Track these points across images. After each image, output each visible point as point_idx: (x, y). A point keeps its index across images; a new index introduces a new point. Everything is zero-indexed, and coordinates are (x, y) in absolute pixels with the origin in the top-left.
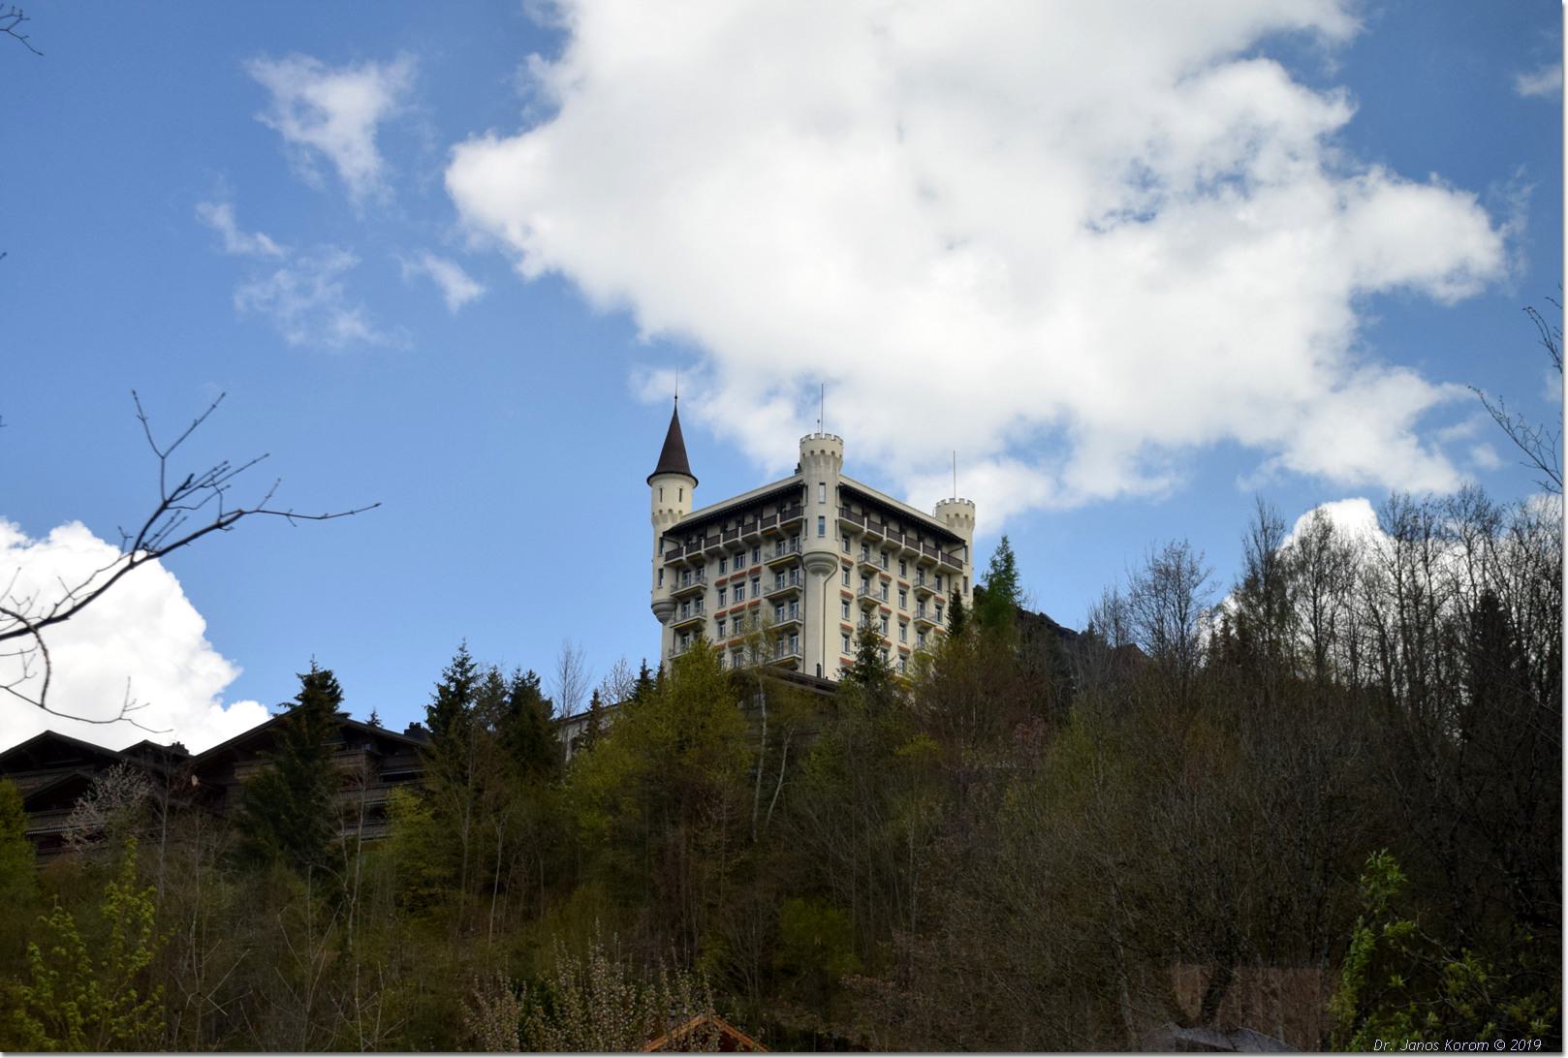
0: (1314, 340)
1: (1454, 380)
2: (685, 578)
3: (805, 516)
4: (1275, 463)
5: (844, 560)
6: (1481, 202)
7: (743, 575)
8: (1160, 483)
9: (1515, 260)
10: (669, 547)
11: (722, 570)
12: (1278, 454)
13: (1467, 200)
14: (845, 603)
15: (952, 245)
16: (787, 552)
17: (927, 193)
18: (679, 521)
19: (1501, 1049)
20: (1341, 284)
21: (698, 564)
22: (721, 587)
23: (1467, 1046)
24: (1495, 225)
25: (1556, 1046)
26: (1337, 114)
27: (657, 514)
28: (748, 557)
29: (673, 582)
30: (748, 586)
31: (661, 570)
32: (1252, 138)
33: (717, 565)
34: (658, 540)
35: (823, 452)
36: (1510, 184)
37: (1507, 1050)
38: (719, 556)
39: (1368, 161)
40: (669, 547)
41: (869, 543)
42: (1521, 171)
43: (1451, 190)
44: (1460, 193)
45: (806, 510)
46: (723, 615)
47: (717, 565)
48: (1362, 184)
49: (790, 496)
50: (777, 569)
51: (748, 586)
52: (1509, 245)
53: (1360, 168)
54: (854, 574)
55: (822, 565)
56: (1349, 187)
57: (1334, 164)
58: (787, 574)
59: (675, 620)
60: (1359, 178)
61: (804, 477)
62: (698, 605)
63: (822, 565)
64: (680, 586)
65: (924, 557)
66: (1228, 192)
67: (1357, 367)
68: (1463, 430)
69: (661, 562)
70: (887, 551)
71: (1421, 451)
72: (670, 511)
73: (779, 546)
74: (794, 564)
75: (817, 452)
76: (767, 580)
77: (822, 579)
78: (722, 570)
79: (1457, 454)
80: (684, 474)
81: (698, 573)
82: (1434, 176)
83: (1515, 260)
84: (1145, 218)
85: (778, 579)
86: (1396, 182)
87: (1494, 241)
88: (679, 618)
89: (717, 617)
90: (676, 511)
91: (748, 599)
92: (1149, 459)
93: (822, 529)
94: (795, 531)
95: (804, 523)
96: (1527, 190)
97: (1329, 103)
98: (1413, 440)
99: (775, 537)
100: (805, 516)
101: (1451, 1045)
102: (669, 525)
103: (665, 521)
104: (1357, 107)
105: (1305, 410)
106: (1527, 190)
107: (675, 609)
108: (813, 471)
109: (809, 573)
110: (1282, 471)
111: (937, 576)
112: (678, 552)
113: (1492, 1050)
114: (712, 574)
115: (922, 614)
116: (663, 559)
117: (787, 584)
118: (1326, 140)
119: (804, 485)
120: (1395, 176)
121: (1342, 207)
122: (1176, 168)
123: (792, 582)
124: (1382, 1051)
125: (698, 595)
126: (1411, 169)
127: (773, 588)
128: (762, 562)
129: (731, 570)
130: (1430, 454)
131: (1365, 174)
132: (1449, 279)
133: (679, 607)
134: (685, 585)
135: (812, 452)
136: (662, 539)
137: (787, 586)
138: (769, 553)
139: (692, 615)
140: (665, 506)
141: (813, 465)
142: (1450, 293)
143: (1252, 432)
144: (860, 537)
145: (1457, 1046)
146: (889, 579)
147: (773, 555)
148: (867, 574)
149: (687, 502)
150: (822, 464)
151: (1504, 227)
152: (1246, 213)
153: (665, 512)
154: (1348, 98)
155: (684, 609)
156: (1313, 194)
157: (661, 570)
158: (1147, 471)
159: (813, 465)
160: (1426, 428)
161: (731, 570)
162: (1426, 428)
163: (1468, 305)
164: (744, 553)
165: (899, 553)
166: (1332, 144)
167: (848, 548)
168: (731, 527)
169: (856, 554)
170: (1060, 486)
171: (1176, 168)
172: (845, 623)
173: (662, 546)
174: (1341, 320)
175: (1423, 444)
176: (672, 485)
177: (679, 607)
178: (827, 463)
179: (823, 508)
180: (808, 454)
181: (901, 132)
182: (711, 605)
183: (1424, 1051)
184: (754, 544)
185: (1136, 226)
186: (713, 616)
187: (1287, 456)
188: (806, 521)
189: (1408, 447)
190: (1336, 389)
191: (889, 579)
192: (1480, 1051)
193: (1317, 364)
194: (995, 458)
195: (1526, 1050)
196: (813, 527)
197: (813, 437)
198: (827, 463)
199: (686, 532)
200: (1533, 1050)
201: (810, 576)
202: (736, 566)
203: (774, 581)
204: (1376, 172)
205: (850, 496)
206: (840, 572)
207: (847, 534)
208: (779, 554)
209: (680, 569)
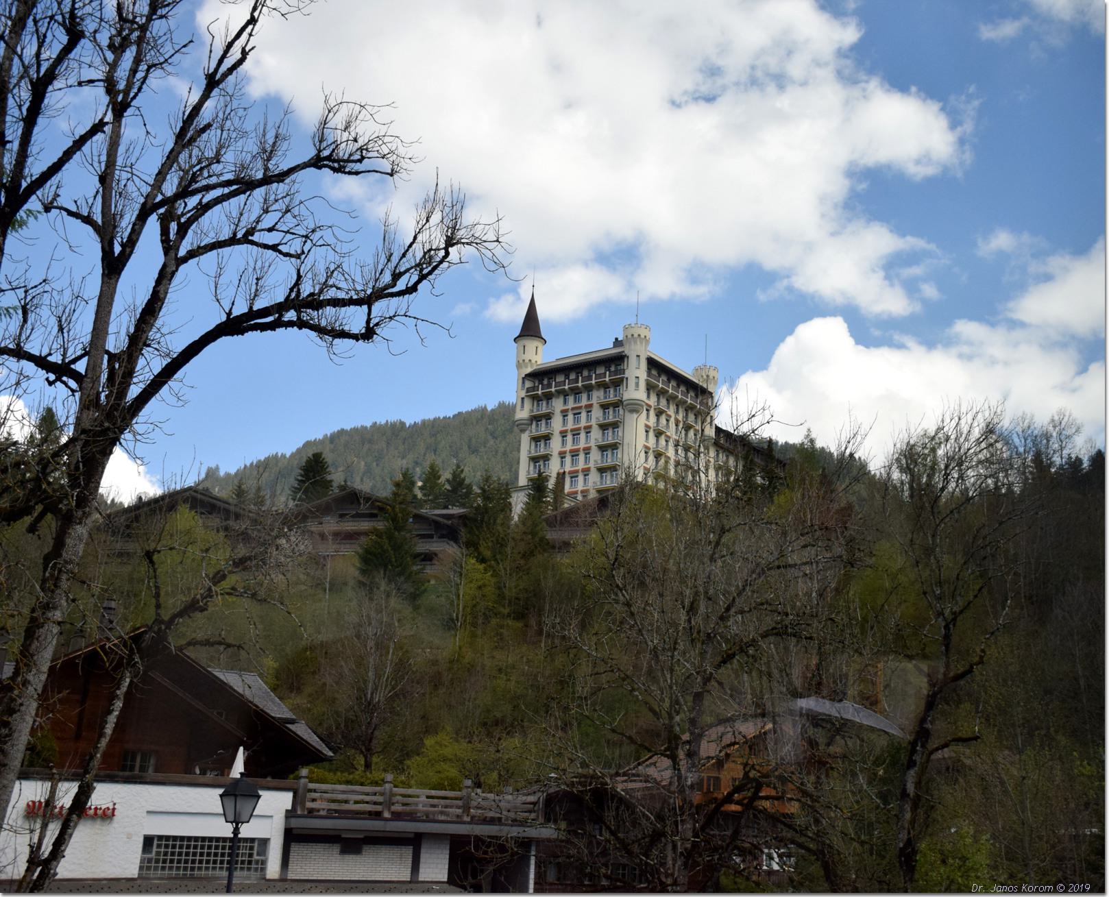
0: (822, 199)
1: (913, 235)
2: (538, 405)
3: (626, 376)
4: (785, 282)
5: (647, 405)
6: (943, 109)
7: (580, 408)
8: (702, 291)
9: (963, 152)
10: (528, 384)
11: (565, 402)
12: (788, 277)
13: (934, 107)
14: (647, 431)
15: (569, 105)
16: (612, 397)
17: (557, 67)
18: (535, 367)
19: (1062, 890)
20: (841, 156)
21: (548, 397)
22: (564, 413)
23: (1037, 888)
24: (953, 125)
25: (1102, 890)
26: (849, 34)
27: (521, 362)
28: (584, 396)
29: (530, 407)
30: (584, 415)
31: (523, 399)
32: (787, 47)
33: (561, 400)
34: (521, 381)
35: (639, 335)
36: (963, 97)
37: (1066, 892)
38: (565, 394)
39: (871, 72)
40: (528, 384)
41: (661, 393)
42: (972, 89)
43: (924, 100)
44: (929, 101)
45: (627, 372)
46: (566, 431)
47: (561, 400)
48: (864, 90)
49: (615, 361)
50: (604, 407)
51: (584, 415)
52: (962, 142)
53: (865, 78)
54: (652, 413)
55: (635, 407)
56: (856, 92)
57: (847, 72)
58: (611, 410)
59: (531, 431)
60: (863, 85)
61: (626, 350)
62: (547, 423)
63: (635, 407)
64: (535, 410)
65: (662, 388)
66: (771, 88)
67: (850, 220)
68: (916, 271)
69: (523, 394)
70: (671, 399)
71: (887, 282)
72: (530, 360)
73: (605, 392)
74: (616, 405)
75: (636, 335)
76: (597, 413)
77: (635, 416)
78: (565, 402)
79: (911, 288)
80: (536, 336)
81: (548, 403)
82: (913, 89)
83: (963, 152)
84: (710, 99)
85: (604, 413)
86: (888, 91)
87: (950, 138)
88: (534, 431)
89: (561, 432)
90: (533, 361)
91: (583, 423)
92: (695, 272)
93: (637, 385)
94: (618, 383)
95: (625, 380)
96: (976, 103)
97: (844, 25)
98: (882, 274)
99: (604, 386)
100: (626, 376)
101: (1027, 888)
102: (529, 370)
103: (526, 367)
104: (863, 31)
105: (809, 247)
106: (976, 103)
107: (531, 424)
108: (633, 347)
109: (626, 412)
110: (790, 289)
111: (695, 415)
112: (534, 388)
113: (1055, 891)
114: (558, 405)
115: (658, 425)
116: (525, 391)
117: (611, 417)
118: (841, 53)
119: (625, 356)
120: (887, 86)
121: (847, 102)
122: (735, 65)
123: (615, 417)
124: (977, 892)
125: (548, 417)
126: (899, 82)
127: (601, 419)
128: (594, 401)
129: (571, 403)
130: (892, 285)
131: (867, 82)
132: (918, 162)
133: (534, 423)
134: (538, 410)
135: (633, 335)
136: (523, 378)
137: (611, 419)
138: (598, 396)
139: (543, 430)
140: (527, 357)
141: (633, 343)
142: (920, 172)
143: (772, 259)
144: (667, 396)
145: (1031, 889)
146: (670, 416)
147: (602, 398)
148: (659, 413)
149: (543, 356)
150: (638, 343)
151: (959, 129)
152: (783, 102)
153: (527, 361)
154: (858, 25)
155: (537, 425)
156: (830, 93)
157: (523, 399)
158: (694, 281)
159: (633, 343)
160: (892, 267)
161: (571, 403)
162: (892, 267)
163: (930, 181)
164: (581, 393)
165: (658, 389)
166: (846, 57)
167: (648, 397)
168: (573, 376)
169: (653, 401)
170: (630, 286)
171: (735, 65)
172: (646, 444)
173: (523, 383)
174: (839, 187)
175: (887, 277)
176: (531, 344)
177: (534, 423)
178: (641, 343)
179: (637, 372)
180: (521, 362)
181: (539, 22)
182: (557, 424)
183: (1007, 892)
184: (589, 389)
185: (702, 104)
186: (558, 432)
187: (794, 279)
188: (627, 378)
189: (877, 279)
190: (833, 234)
191: (670, 416)
192: (1047, 892)
193: (823, 216)
194: (586, 264)
195: (1079, 892)
196: (632, 383)
197: (633, 325)
198: (641, 343)
199: (540, 376)
200: (1084, 891)
201: (627, 414)
202: (575, 401)
203: (602, 415)
204: (874, 84)
205: (653, 364)
206: (645, 412)
207: (650, 387)
208: (605, 398)
209: (535, 398)
